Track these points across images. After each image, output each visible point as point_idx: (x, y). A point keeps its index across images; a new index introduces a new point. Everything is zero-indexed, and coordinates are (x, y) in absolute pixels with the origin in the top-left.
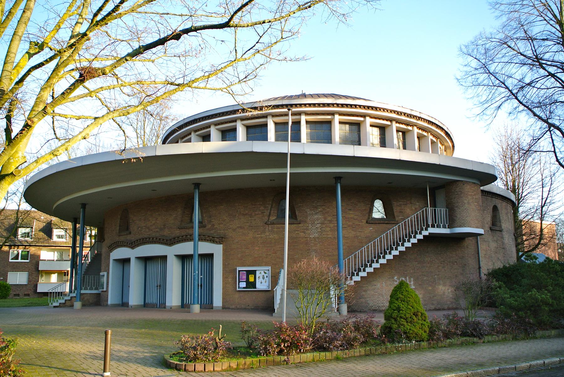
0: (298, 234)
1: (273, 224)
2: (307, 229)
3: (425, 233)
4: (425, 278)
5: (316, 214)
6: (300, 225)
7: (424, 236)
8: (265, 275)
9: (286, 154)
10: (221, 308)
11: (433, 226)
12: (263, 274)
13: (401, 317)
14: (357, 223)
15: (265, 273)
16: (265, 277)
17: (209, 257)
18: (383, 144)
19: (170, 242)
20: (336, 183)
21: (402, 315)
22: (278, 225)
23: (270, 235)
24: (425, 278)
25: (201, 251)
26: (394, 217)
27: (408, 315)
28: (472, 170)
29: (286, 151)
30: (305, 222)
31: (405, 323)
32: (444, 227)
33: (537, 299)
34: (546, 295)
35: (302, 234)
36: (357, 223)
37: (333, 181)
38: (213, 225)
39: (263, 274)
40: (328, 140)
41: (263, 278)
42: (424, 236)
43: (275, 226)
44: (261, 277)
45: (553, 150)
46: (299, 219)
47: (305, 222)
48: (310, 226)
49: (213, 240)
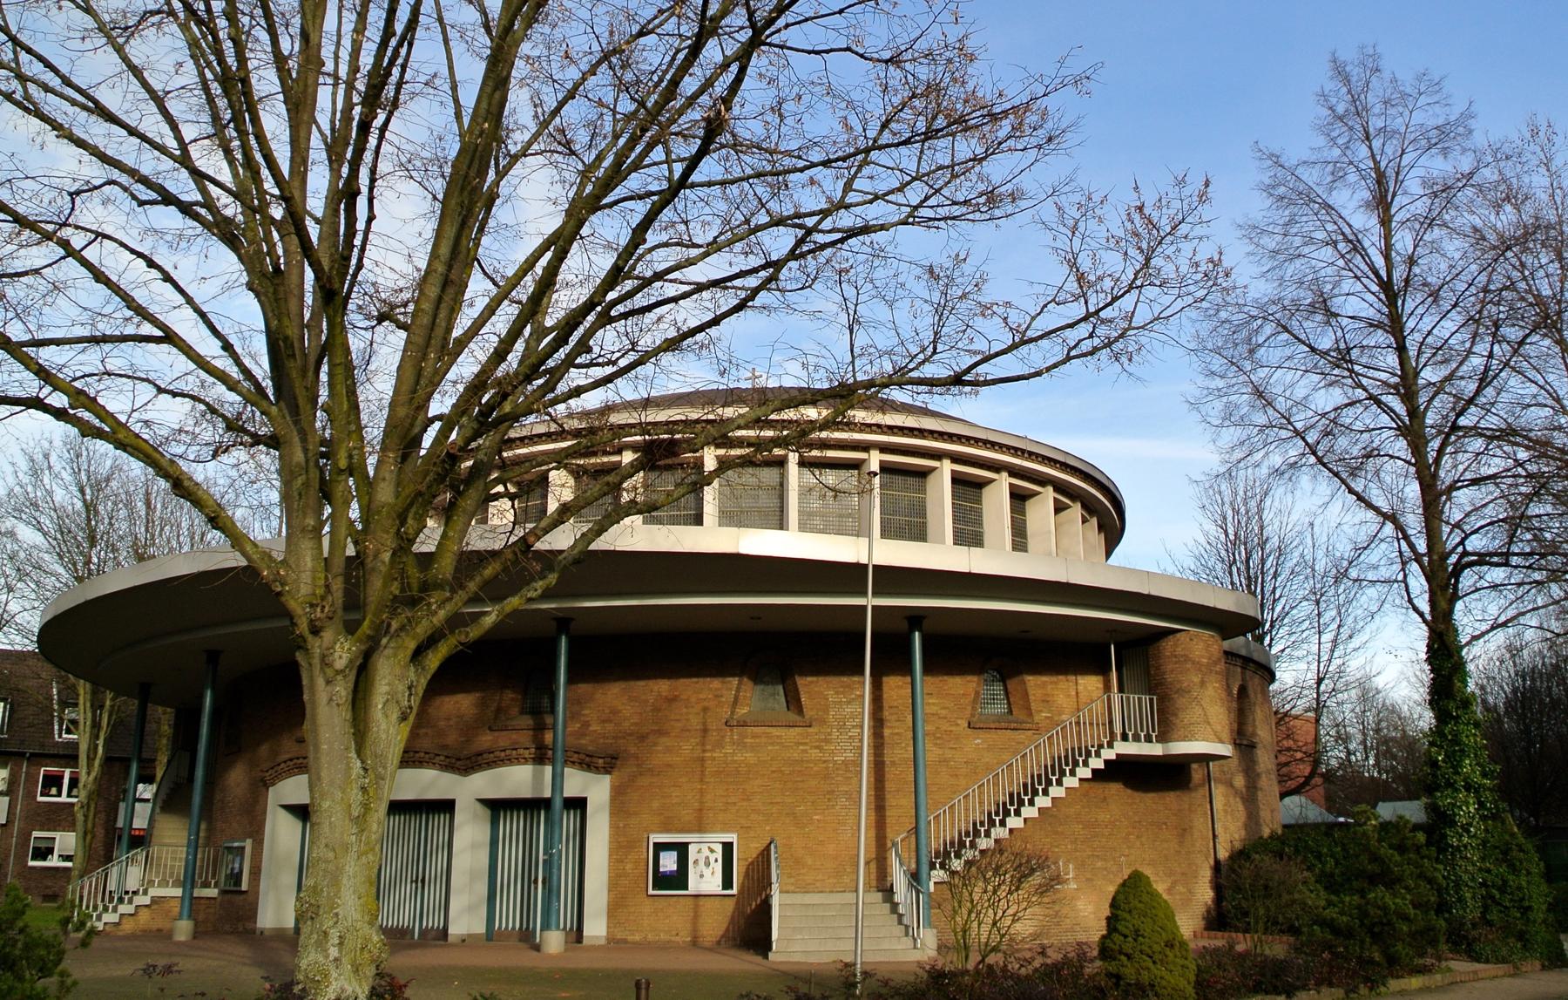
0: (805, 751)
1: (745, 725)
2: (827, 741)
3: (1109, 754)
4: (1099, 864)
5: (849, 703)
6: (810, 730)
7: (1106, 762)
8: (712, 858)
9: (866, 566)
10: (603, 942)
11: (1125, 738)
12: (708, 853)
13: (1141, 952)
14: (945, 726)
15: (712, 851)
16: (712, 861)
17: (578, 805)
18: (1020, 539)
19: (465, 763)
20: (911, 632)
21: (1145, 948)
22: (756, 730)
23: (733, 754)
24: (1099, 864)
25: (569, 792)
26: (1031, 714)
27: (1156, 948)
28: (1215, 609)
29: (864, 561)
30: (823, 722)
31: (1150, 965)
32: (1148, 739)
33: (1385, 908)
34: (1404, 898)
35: (814, 754)
36: (945, 726)
37: (905, 625)
38: (586, 724)
39: (706, 852)
40: (917, 532)
41: (707, 864)
42: (1106, 762)
43: (749, 729)
44: (702, 863)
45: (1400, 577)
46: (809, 713)
47: (823, 722)
48: (835, 734)
49: (588, 763)
